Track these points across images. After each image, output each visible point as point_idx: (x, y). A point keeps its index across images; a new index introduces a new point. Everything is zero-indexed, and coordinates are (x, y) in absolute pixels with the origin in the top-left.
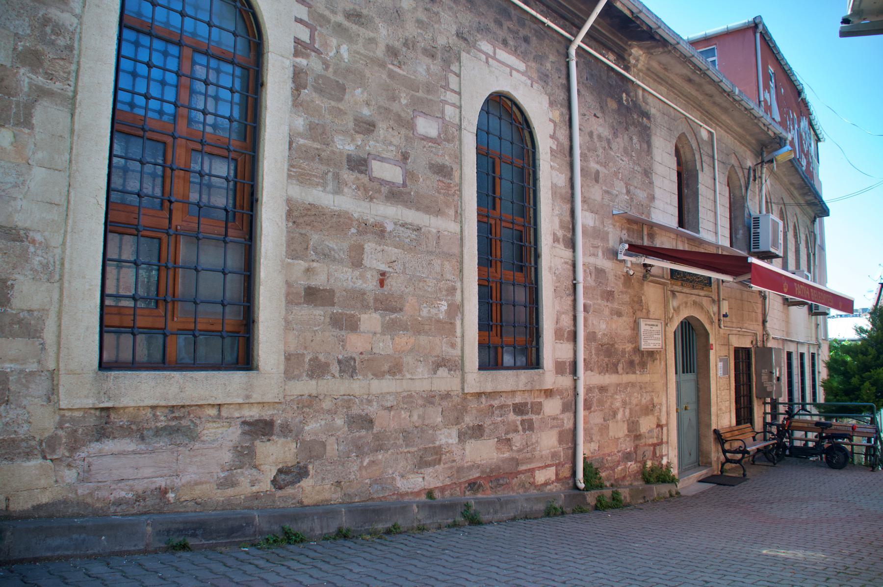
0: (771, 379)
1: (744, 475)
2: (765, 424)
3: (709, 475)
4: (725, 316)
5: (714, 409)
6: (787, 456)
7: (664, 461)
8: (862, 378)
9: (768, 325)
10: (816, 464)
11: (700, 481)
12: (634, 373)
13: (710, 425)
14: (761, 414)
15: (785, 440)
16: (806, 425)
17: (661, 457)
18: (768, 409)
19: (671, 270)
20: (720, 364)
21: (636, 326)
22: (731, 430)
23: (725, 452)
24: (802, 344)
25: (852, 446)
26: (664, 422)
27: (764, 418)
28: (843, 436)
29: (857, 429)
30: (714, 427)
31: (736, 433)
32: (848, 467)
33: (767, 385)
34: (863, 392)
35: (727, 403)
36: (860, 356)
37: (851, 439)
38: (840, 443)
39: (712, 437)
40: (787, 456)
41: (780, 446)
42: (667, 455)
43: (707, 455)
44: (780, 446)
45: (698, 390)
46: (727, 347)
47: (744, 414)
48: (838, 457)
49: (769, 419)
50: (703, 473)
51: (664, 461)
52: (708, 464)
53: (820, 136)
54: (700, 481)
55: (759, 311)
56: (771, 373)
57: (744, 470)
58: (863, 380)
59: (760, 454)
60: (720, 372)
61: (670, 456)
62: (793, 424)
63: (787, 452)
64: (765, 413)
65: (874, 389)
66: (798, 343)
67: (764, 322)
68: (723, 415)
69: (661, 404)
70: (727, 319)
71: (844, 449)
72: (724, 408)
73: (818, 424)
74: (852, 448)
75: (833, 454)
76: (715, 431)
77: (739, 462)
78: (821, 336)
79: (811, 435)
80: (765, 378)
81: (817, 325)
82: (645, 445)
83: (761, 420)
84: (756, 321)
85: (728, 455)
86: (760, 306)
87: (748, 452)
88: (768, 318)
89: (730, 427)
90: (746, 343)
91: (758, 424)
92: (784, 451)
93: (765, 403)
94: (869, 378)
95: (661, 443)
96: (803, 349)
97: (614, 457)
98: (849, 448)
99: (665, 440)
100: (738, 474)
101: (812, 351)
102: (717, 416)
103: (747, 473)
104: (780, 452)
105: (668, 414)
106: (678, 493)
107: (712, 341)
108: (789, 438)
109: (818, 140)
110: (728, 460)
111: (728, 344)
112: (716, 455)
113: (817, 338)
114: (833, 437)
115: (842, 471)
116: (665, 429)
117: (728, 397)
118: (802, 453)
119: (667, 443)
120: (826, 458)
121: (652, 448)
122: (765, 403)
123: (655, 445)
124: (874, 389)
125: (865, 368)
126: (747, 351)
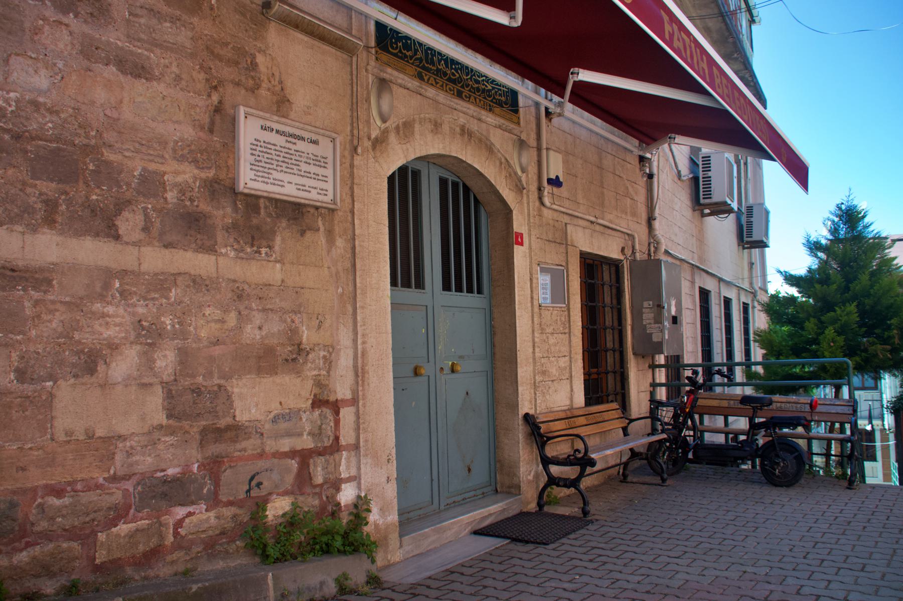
0: (658, 320)
1: (585, 513)
2: (655, 404)
3: (511, 513)
4: (555, 182)
5: (524, 372)
6: (690, 461)
7: (347, 495)
8: (822, 322)
9: (657, 224)
10: (746, 478)
11: (476, 533)
12: (211, 250)
13: (515, 406)
14: (646, 386)
15: (686, 432)
16: (725, 404)
17: (336, 485)
18: (661, 376)
19: (380, 27)
20: (544, 280)
21: (221, 123)
22: (569, 416)
23: (546, 462)
24: (728, 283)
25: (809, 440)
26: (342, 390)
27: (652, 394)
28: (793, 422)
29: (819, 408)
30: (525, 407)
31: (582, 421)
32: (802, 481)
33: (652, 329)
34: (824, 345)
35: (563, 362)
36: (818, 286)
37: (807, 427)
38: (786, 436)
39: (520, 431)
40: (690, 461)
41: (677, 441)
42: (355, 479)
43: (511, 470)
44: (677, 441)
45: (492, 332)
46: (562, 249)
47: (603, 382)
48: (785, 463)
49: (662, 394)
50: (493, 510)
51: (347, 495)
52: (513, 489)
53: (756, 19)
54: (476, 533)
55: (641, 198)
56: (660, 307)
57: (585, 503)
58: (822, 326)
59: (637, 463)
60: (544, 295)
61: (370, 482)
62: (701, 402)
63: (690, 456)
64: (654, 385)
65: (841, 340)
66: (720, 280)
67: (650, 219)
68: (551, 380)
69: (332, 348)
70: (563, 191)
71: (794, 448)
72: (554, 371)
73: (745, 400)
74: (810, 446)
75: (776, 461)
76: (527, 417)
77: (573, 483)
78: (758, 284)
79: (741, 423)
80: (648, 317)
81: (751, 264)
82: (261, 455)
83: (646, 397)
84: (634, 214)
85: (555, 469)
86: (642, 192)
87: (592, 463)
88: (657, 212)
89: (571, 409)
90: (610, 249)
91: (639, 403)
92: (685, 453)
93: (653, 367)
94: (835, 321)
95: (335, 447)
96: (731, 294)
97: (92, 496)
98: (802, 443)
99: (347, 436)
100: (573, 510)
101: (743, 299)
102: (535, 386)
103: (591, 508)
104: (675, 456)
105: (359, 373)
106: (374, 581)
107: (519, 224)
108: (694, 428)
109: (752, 21)
110: (553, 481)
111: (562, 241)
112: (528, 470)
113: (751, 284)
114: (773, 423)
115: (792, 492)
116: (347, 414)
117: (565, 350)
118: (723, 458)
119: (356, 447)
120: (762, 464)
121: (294, 464)
122: (653, 367)
123: (304, 457)
124: (841, 340)
125: (826, 305)
126: (616, 266)
